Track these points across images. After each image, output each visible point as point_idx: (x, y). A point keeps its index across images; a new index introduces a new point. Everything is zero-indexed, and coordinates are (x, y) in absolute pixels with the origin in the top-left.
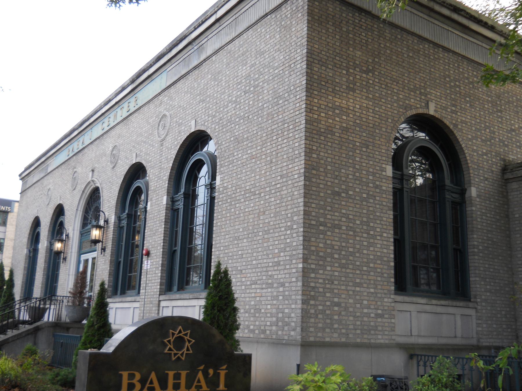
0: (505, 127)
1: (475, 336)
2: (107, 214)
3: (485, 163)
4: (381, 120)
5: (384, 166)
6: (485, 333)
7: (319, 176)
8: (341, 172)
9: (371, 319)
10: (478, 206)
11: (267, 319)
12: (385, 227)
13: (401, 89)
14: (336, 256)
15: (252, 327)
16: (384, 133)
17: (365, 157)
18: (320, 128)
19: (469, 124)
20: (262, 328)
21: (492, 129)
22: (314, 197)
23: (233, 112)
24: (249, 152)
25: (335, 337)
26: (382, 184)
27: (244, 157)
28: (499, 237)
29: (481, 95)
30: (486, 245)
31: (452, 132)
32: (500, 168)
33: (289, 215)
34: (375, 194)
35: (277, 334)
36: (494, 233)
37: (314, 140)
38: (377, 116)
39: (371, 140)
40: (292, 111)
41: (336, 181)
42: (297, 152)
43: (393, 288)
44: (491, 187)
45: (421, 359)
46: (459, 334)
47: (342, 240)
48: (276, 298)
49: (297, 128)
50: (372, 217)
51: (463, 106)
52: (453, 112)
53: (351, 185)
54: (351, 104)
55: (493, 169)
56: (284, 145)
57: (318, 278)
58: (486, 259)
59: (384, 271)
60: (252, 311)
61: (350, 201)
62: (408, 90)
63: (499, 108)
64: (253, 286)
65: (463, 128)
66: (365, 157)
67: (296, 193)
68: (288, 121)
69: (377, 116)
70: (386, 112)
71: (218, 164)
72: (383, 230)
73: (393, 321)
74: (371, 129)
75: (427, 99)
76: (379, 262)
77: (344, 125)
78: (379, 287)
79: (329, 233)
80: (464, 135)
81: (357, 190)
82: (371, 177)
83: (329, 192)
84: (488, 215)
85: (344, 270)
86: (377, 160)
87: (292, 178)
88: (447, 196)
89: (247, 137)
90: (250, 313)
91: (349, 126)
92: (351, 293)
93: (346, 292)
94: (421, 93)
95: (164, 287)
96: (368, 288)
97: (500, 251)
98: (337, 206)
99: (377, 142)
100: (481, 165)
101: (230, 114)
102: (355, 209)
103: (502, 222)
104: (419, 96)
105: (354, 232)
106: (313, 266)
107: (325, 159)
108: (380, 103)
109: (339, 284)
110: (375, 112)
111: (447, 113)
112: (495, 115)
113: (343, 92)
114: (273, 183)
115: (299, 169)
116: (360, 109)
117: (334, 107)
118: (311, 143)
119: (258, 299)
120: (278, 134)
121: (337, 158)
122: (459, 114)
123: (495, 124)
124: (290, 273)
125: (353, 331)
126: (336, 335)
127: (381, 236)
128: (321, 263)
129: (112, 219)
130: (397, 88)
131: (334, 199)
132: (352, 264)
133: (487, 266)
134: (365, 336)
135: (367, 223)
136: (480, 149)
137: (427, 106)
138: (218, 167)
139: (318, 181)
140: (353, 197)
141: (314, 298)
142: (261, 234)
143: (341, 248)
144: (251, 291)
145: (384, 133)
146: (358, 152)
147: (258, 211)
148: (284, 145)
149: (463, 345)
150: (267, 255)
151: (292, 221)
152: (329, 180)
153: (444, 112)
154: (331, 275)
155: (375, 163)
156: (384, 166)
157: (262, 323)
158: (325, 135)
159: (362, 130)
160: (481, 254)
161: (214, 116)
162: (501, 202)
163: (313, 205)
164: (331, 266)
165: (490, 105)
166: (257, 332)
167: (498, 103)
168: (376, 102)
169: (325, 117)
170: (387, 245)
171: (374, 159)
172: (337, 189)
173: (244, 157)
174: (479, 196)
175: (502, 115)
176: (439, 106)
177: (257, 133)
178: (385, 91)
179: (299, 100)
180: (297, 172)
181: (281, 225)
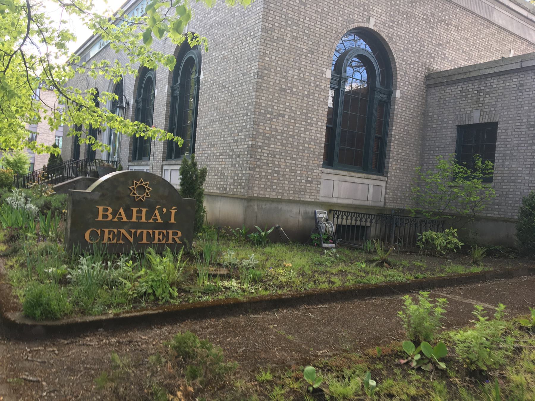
0: (434, 42)
1: (383, 200)
2: (127, 98)
3: (412, 71)
4: (327, 31)
5: (325, 69)
6: (391, 199)
7: (270, 75)
8: (288, 73)
9: (302, 184)
10: (400, 105)
11: (228, 180)
12: (320, 118)
13: (347, 5)
14: (279, 137)
15: (218, 186)
16: (328, 43)
17: (309, 62)
18: (274, 36)
19: (403, 38)
20: (225, 186)
21: (422, 43)
22: (264, 92)
23: (214, 18)
24: (223, 53)
25: (274, 195)
26: (321, 84)
27: (220, 57)
28: (414, 130)
29: (417, 14)
30: (401, 135)
31: (387, 44)
32: (424, 76)
33: (246, 105)
34: (315, 92)
35: (233, 191)
36: (410, 126)
37: (268, 45)
38: (323, 28)
39: (316, 48)
40: (253, 20)
41: (284, 80)
42: (254, 55)
43: (322, 163)
44: (414, 90)
45: (369, 217)
46: (370, 198)
47: (285, 126)
48: (234, 166)
49: (256, 35)
50: (310, 109)
51: (400, 22)
52: (390, 27)
53: (295, 83)
54: (302, 17)
55: (418, 76)
56: (246, 49)
57: (264, 153)
58: (400, 145)
59: (316, 150)
60: (219, 174)
61: (294, 96)
62: (353, 6)
63: (432, 25)
64: (221, 157)
65: (397, 41)
66: (309, 62)
67: (251, 88)
68: (250, 28)
69: (323, 28)
70: (332, 25)
71: (202, 61)
72: (318, 120)
73: (319, 186)
74: (317, 39)
75: (369, 15)
76: (312, 143)
77: (294, 34)
78: (311, 162)
79: (274, 120)
80: (396, 46)
81: (301, 88)
82: (313, 78)
83: (277, 88)
84: (408, 112)
85: (284, 148)
86: (320, 65)
87: (249, 75)
88: (376, 96)
89: (223, 40)
90: (218, 176)
91: (298, 35)
92: (288, 164)
93: (284, 164)
94: (364, 10)
95: (166, 155)
96: (301, 162)
97: (413, 140)
98: (282, 99)
99: (321, 49)
100: (408, 73)
101: (212, 20)
102: (297, 103)
103: (419, 118)
104: (363, 12)
105: (295, 120)
106: (260, 144)
107: (275, 61)
108: (328, 17)
109: (279, 158)
110: (322, 24)
111: (385, 28)
112: (427, 31)
113: (295, 6)
114: (237, 79)
115: (255, 69)
116: (309, 21)
117: (287, 18)
118: (265, 48)
119: (223, 166)
120: (243, 39)
121: (286, 61)
122: (395, 29)
123: (426, 38)
124: (244, 148)
125: (287, 192)
126: (274, 194)
127: (316, 124)
128: (266, 142)
129: (132, 102)
130: (344, 4)
131: (281, 94)
132: (291, 144)
133: (400, 151)
134: (297, 195)
135: (306, 115)
136: (409, 59)
137: (368, 21)
138: (202, 64)
139: (269, 79)
140: (297, 93)
141: (259, 167)
142: (227, 118)
143: (283, 131)
144: (220, 160)
145: (328, 43)
146: (304, 57)
147: (226, 101)
148: (246, 49)
149: (372, 206)
150: (231, 134)
151: (248, 109)
152: (278, 79)
153: (382, 26)
154: (274, 151)
155: (318, 67)
156: (325, 69)
157: (225, 183)
158: (278, 42)
159: (309, 39)
160: (396, 142)
161: (201, 21)
162: (420, 103)
163: (263, 98)
164: (274, 144)
165: (424, 22)
166: (221, 189)
167: (432, 20)
168: (324, 15)
169: (279, 27)
170: (320, 131)
171: (316, 64)
172: (283, 87)
173: (220, 57)
174: (401, 97)
175: (434, 32)
176: (378, 22)
177: (229, 37)
178: (333, 6)
179: (259, 11)
180: (253, 71)
181: (241, 112)
